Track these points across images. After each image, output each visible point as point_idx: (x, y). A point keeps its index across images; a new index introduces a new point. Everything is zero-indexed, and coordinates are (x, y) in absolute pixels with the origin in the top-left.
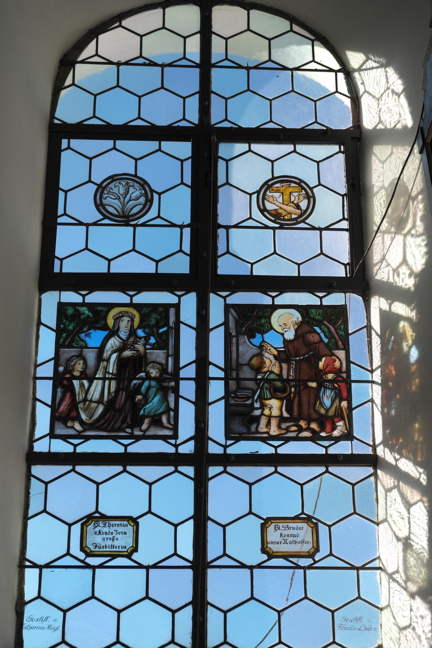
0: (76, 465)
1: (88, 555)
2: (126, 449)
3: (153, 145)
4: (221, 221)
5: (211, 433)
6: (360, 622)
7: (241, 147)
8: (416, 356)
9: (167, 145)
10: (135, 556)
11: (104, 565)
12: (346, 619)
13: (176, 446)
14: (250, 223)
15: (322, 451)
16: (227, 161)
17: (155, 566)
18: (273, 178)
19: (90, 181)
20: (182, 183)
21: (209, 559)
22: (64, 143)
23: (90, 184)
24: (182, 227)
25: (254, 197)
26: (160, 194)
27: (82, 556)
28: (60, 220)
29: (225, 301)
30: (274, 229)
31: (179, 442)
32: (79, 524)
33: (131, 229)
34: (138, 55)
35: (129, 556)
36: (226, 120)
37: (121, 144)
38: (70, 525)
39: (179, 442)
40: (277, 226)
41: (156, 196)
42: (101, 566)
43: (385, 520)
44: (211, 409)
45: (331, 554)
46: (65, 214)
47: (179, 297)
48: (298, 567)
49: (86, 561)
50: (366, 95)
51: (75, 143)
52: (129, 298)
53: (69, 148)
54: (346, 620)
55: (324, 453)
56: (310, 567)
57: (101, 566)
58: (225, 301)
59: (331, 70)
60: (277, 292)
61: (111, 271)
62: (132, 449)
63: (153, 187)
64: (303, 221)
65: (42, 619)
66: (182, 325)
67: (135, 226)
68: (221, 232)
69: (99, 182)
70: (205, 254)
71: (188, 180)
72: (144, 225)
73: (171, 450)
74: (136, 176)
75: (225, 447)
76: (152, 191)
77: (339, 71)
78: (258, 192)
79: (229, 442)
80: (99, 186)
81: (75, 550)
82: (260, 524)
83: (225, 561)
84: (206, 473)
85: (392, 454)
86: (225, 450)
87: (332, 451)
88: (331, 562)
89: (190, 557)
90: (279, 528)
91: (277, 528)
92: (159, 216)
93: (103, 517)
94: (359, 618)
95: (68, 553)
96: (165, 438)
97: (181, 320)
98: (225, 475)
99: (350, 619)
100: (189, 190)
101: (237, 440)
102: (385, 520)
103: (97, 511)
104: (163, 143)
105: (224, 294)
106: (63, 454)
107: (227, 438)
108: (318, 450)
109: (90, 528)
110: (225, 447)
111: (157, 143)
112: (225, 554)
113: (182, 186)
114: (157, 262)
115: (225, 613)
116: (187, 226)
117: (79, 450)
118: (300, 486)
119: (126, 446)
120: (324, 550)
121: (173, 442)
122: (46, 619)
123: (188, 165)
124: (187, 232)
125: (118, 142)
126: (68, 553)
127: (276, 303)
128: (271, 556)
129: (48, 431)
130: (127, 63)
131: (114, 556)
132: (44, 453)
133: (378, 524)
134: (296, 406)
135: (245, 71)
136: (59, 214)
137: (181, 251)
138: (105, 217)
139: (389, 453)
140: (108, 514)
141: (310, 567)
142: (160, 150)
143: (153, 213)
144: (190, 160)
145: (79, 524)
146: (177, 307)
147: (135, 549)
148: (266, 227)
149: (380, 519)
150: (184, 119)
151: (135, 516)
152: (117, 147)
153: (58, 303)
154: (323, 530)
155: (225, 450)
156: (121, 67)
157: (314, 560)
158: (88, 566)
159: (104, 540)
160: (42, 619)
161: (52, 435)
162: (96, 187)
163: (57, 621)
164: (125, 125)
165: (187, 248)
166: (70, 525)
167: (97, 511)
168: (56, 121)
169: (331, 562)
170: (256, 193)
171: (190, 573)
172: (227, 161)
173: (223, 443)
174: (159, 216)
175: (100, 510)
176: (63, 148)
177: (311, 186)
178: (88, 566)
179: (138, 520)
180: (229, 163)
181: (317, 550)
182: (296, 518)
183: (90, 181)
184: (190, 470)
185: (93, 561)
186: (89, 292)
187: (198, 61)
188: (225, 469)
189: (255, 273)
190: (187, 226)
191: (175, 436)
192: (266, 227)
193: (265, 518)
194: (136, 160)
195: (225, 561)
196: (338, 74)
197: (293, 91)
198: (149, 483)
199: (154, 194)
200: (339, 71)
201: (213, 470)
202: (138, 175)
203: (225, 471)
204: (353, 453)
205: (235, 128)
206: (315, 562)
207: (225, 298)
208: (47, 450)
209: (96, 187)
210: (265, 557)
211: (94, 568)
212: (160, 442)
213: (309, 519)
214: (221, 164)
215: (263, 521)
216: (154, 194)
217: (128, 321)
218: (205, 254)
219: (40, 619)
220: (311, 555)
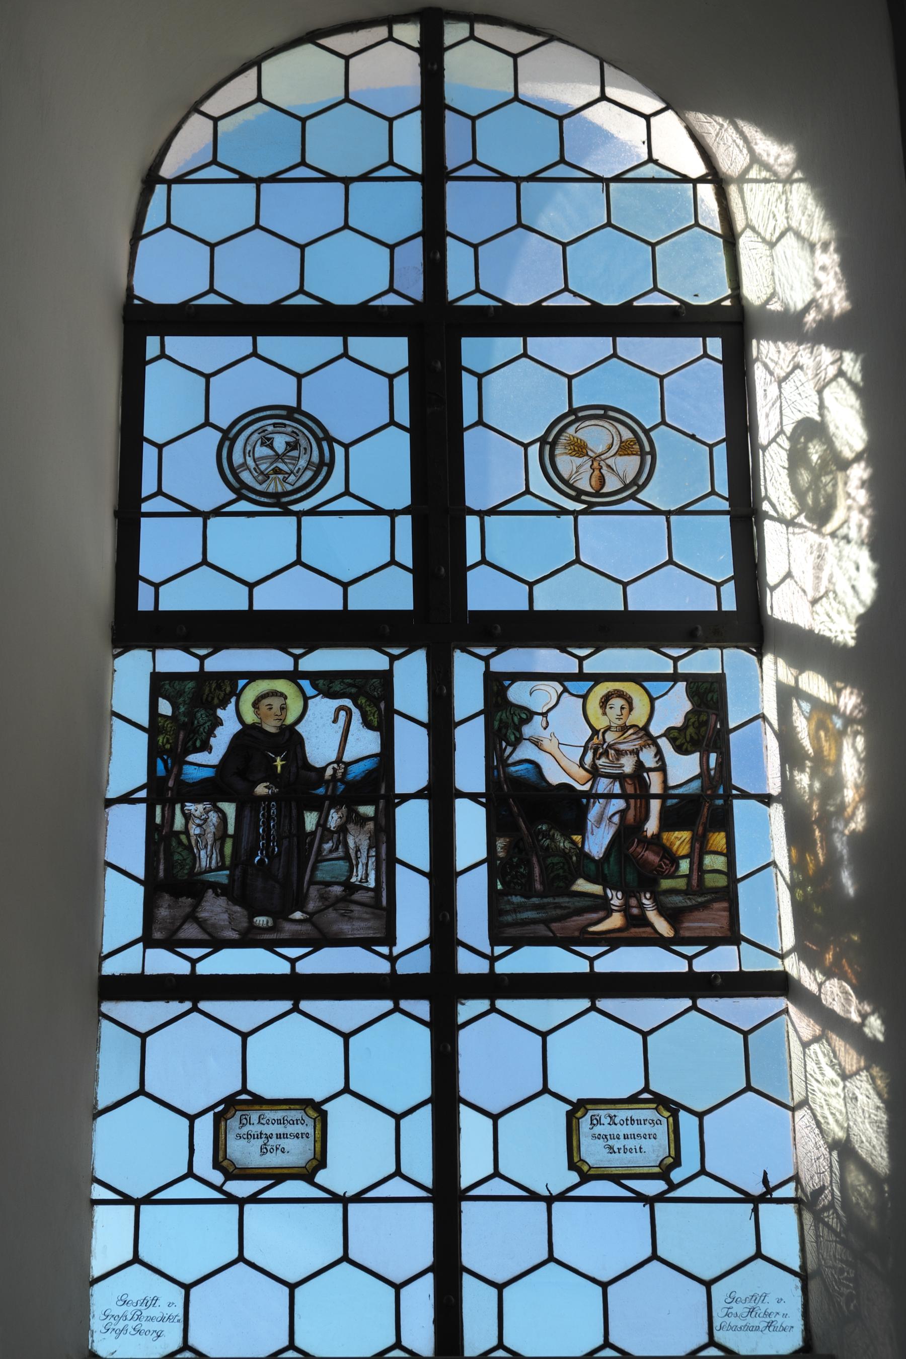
0: (496, 999)
1: (230, 1176)
2: (293, 968)
3: (332, 345)
4: (471, 501)
5: (464, 932)
6: (762, 1302)
7: (511, 345)
8: (356, 776)
9: (360, 345)
10: (321, 1177)
11: (259, 1197)
12: (734, 1299)
13: (392, 959)
14: (527, 503)
15: (682, 967)
16: (480, 377)
17: (359, 1198)
18: (572, 411)
19: (207, 423)
20: (392, 422)
21: (465, 1183)
22: (152, 345)
23: (208, 429)
24: (393, 514)
25: (534, 450)
26: (346, 447)
27: (217, 1178)
28: (145, 507)
29: (487, 666)
30: (576, 514)
31: (396, 951)
32: (210, 1115)
33: (293, 520)
34: (386, 159)
35: (307, 1175)
36: (301, 291)
37: (268, 344)
38: (192, 1118)
39: (396, 951)
40: (582, 506)
41: (339, 451)
42: (254, 1199)
43: (804, 1103)
44: (462, 883)
45: (703, 1172)
46: (160, 492)
47: (393, 659)
48: (640, 1197)
49: (225, 1188)
50: (749, 232)
51: (176, 345)
52: (197, 662)
53: (163, 355)
54: (735, 1300)
55: (588, 970)
56: (661, 1198)
57: (254, 1199)
58: (487, 666)
59: (685, 179)
60: (685, 648)
61: (256, 607)
62: (305, 967)
63: (334, 433)
64: (633, 497)
65: (145, 1301)
66: (397, 718)
67: (299, 515)
68: (472, 523)
69: (225, 426)
70: (443, 570)
71: (403, 415)
72: (313, 512)
73: (383, 967)
74: (298, 409)
75: (493, 959)
76: (331, 440)
77: (702, 180)
78: (542, 440)
79: (499, 950)
80: (225, 433)
81: (204, 1165)
82: (565, 1113)
83: (497, 1187)
84: (454, 1014)
85: (810, 972)
86: (492, 967)
87: (702, 965)
88: (703, 1187)
89: (427, 1179)
90: (599, 1122)
91: (595, 1122)
92: (347, 492)
93: (258, 1101)
94: (152, 1298)
95: (190, 1173)
96: (367, 944)
97: (396, 707)
98: (295, 1015)
99: (743, 1298)
100: (146, 434)
101: (516, 944)
102: (804, 1103)
103: (244, 1090)
104: (351, 340)
105: (485, 652)
106: (388, 978)
107: (493, 942)
108: (676, 965)
109: (233, 1123)
110: (493, 959)
111: (249, 339)
112: (496, 1174)
113: (392, 428)
114: (345, 586)
115: (500, 1287)
116: (405, 511)
117: (203, 969)
118: (742, 1036)
119: (293, 962)
120: (690, 1163)
121: (385, 950)
122: (154, 1302)
123: (402, 384)
124: (405, 524)
125: (260, 340)
126: (190, 1173)
127: (680, 671)
128: (585, 1178)
129: (138, 932)
130: (365, 177)
131: (279, 1176)
132: (422, 974)
133: (793, 1110)
134: (538, 878)
135: (513, 185)
136: (144, 494)
137: (393, 562)
138: (240, 497)
139: (806, 970)
140: (268, 1094)
141: (661, 1198)
142: (525, 355)
143: (335, 485)
144: (406, 375)
145: (210, 1115)
146: (386, 677)
147: (320, 1161)
148: (563, 511)
149: (798, 1098)
150: (212, 290)
151: (318, 1098)
152: (260, 351)
153: (151, 673)
154: (688, 1123)
155: (492, 967)
156: (353, 187)
157: (669, 1181)
158: (230, 1199)
159: (606, 1140)
160: (145, 1301)
161: (148, 940)
162: (219, 435)
163: (174, 1305)
164: (277, 305)
165: (405, 555)
166: (192, 1118)
167: (244, 1090)
168: (136, 302)
169: (703, 1187)
170: (538, 441)
171: (426, 1211)
172: (480, 377)
173: (487, 950)
174: (347, 492)
175: (250, 1087)
176: (148, 357)
177: (647, 427)
178: (230, 1199)
179: (325, 1107)
180: (484, 380)
181: (677, 1162)
182: (633, 1100)
183: (207, 423)
184: (422, 1008)
185: (241, 1188)
186: (406, 649)
187: (418, 168)
188: (593, 1004)
189: (539, 606)
190: (405, 511)
191: (390, 940)
192: (563, 511)
193: (575, 1101)
194: (299, 377)
195: (497, 1187)
196: (700, 187)
197: (609, 224)
198: (541, 1032)
199: (335, 445)
200: (702, 180)
201: (467, 1009)
202: (304, 408)
203: (593, 1008)
204: (744, 969)
205: (495, 307)
206: (672, 1187)
207: (486, 659)
208: (138, 971)
209: (219, 435)
210: (574, 1178)
211: (241, 1202)
212: (358, 951)
213: (661, 1102)
214: (468, 383)
215: (569, 1108)
216: (335, 445)
217: (622, 708)
218: (443, 570)
219: (142, 1301)
220: (664, 1173)
